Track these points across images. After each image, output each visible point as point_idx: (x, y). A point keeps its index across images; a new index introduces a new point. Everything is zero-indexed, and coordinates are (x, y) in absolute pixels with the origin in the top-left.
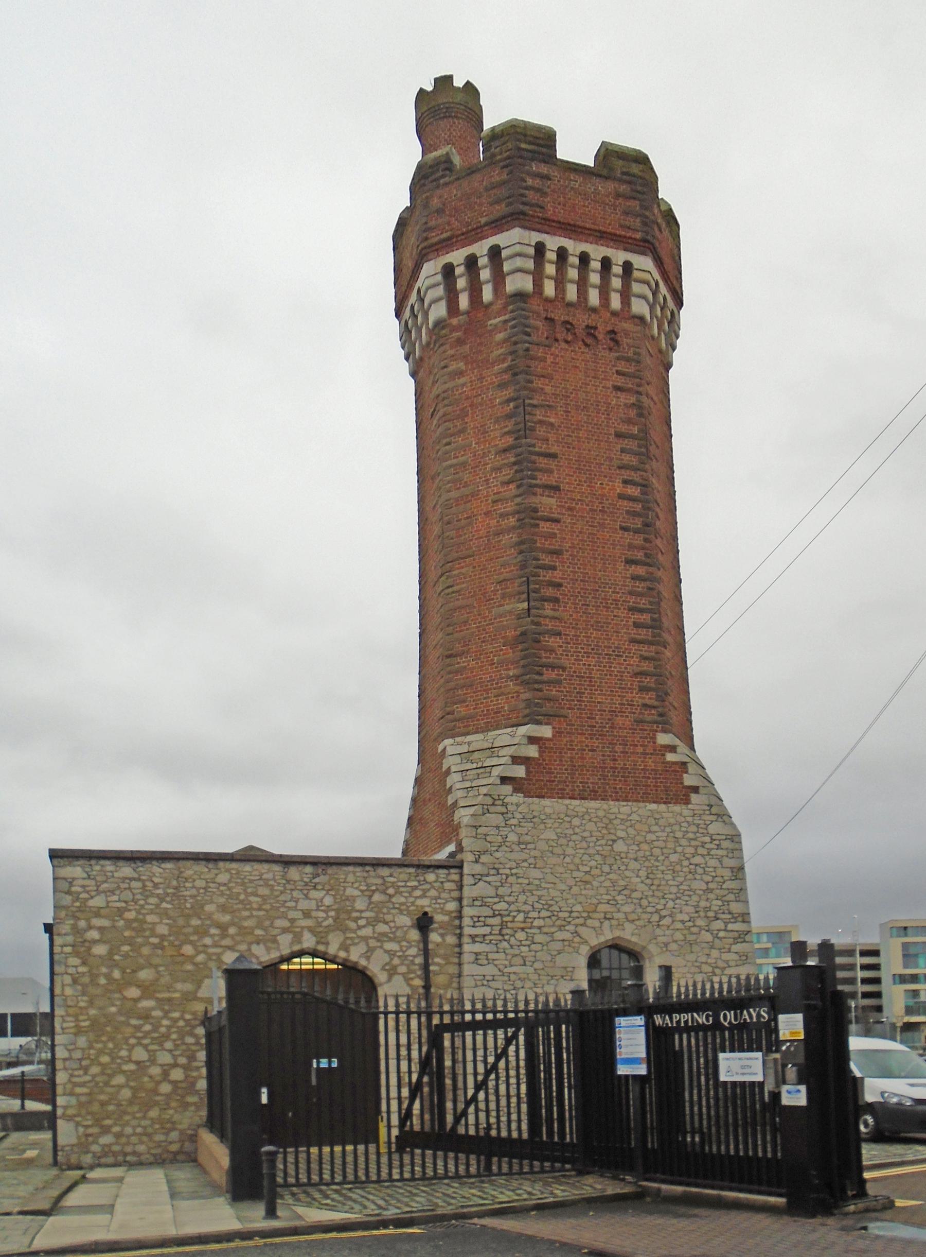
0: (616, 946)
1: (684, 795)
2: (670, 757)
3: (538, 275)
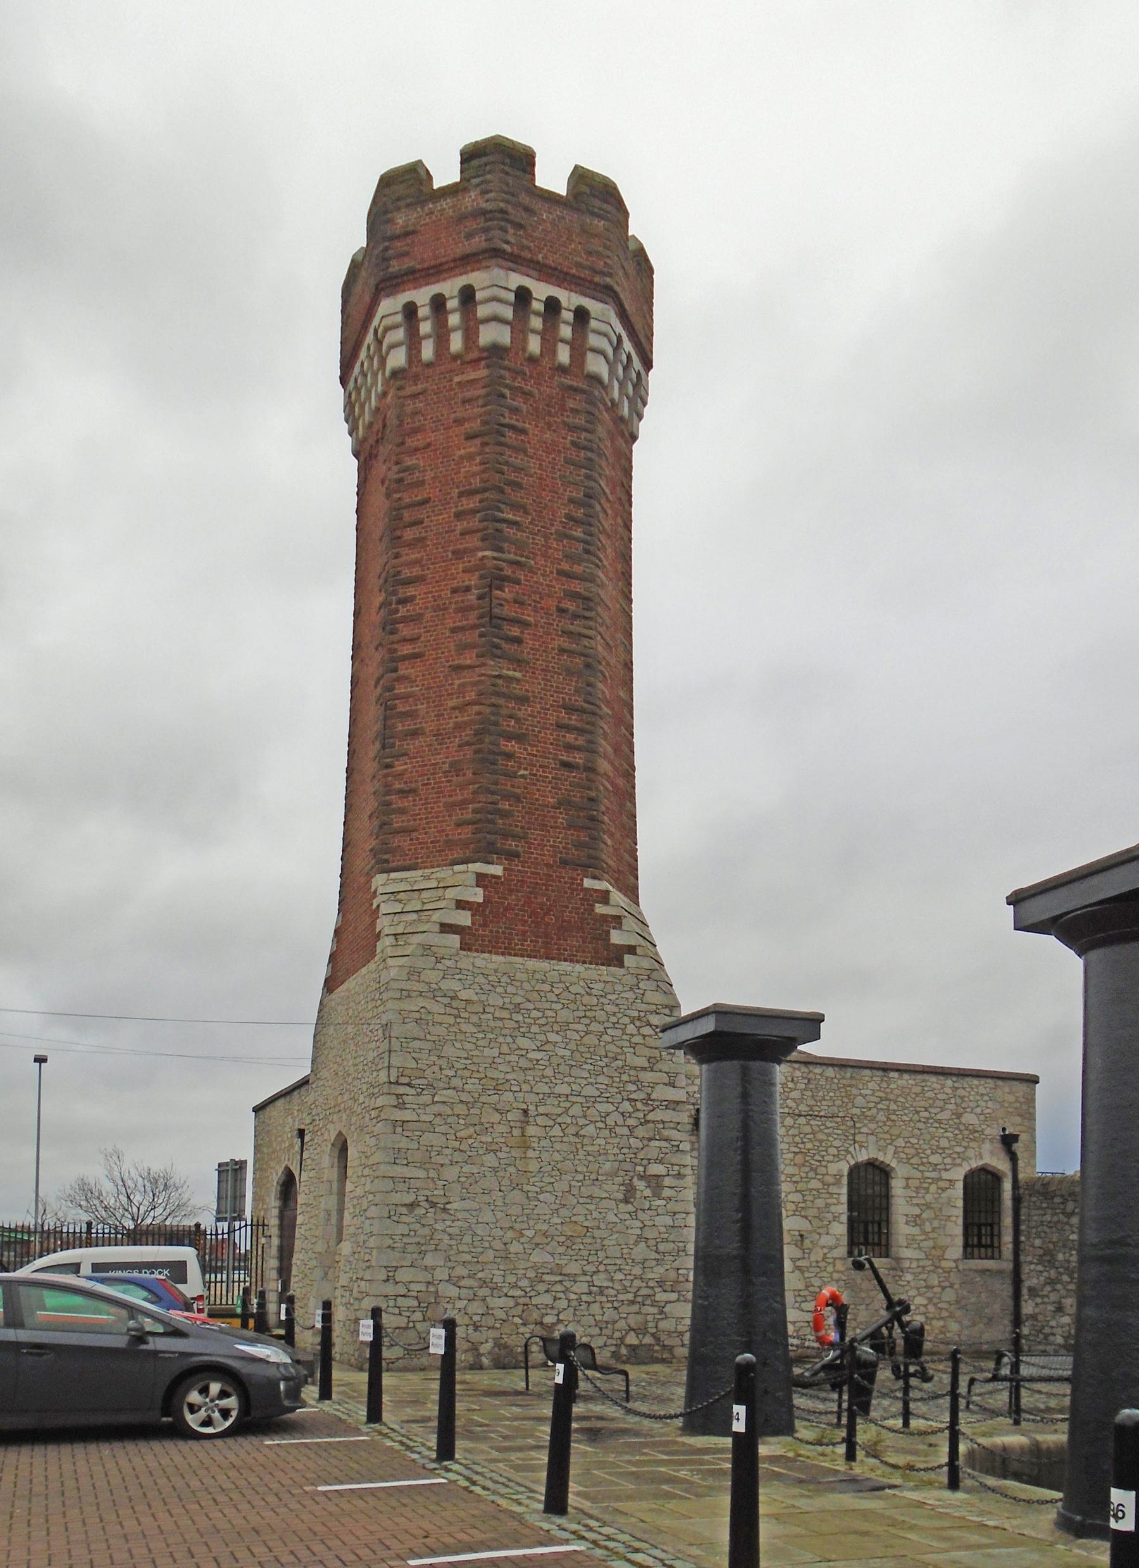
0: (872, 1164)
1: (615, 957)
2: (600, 909)
3: (519, 327)
